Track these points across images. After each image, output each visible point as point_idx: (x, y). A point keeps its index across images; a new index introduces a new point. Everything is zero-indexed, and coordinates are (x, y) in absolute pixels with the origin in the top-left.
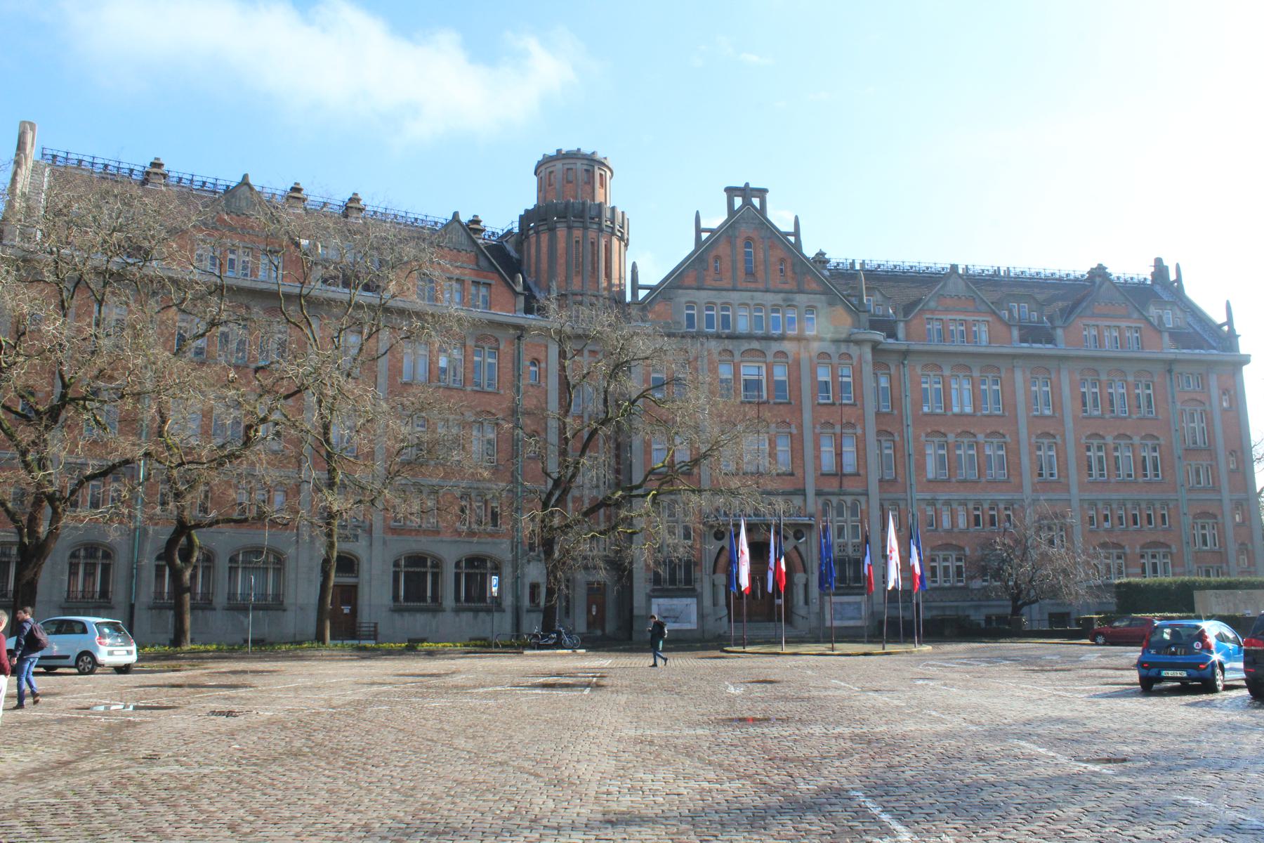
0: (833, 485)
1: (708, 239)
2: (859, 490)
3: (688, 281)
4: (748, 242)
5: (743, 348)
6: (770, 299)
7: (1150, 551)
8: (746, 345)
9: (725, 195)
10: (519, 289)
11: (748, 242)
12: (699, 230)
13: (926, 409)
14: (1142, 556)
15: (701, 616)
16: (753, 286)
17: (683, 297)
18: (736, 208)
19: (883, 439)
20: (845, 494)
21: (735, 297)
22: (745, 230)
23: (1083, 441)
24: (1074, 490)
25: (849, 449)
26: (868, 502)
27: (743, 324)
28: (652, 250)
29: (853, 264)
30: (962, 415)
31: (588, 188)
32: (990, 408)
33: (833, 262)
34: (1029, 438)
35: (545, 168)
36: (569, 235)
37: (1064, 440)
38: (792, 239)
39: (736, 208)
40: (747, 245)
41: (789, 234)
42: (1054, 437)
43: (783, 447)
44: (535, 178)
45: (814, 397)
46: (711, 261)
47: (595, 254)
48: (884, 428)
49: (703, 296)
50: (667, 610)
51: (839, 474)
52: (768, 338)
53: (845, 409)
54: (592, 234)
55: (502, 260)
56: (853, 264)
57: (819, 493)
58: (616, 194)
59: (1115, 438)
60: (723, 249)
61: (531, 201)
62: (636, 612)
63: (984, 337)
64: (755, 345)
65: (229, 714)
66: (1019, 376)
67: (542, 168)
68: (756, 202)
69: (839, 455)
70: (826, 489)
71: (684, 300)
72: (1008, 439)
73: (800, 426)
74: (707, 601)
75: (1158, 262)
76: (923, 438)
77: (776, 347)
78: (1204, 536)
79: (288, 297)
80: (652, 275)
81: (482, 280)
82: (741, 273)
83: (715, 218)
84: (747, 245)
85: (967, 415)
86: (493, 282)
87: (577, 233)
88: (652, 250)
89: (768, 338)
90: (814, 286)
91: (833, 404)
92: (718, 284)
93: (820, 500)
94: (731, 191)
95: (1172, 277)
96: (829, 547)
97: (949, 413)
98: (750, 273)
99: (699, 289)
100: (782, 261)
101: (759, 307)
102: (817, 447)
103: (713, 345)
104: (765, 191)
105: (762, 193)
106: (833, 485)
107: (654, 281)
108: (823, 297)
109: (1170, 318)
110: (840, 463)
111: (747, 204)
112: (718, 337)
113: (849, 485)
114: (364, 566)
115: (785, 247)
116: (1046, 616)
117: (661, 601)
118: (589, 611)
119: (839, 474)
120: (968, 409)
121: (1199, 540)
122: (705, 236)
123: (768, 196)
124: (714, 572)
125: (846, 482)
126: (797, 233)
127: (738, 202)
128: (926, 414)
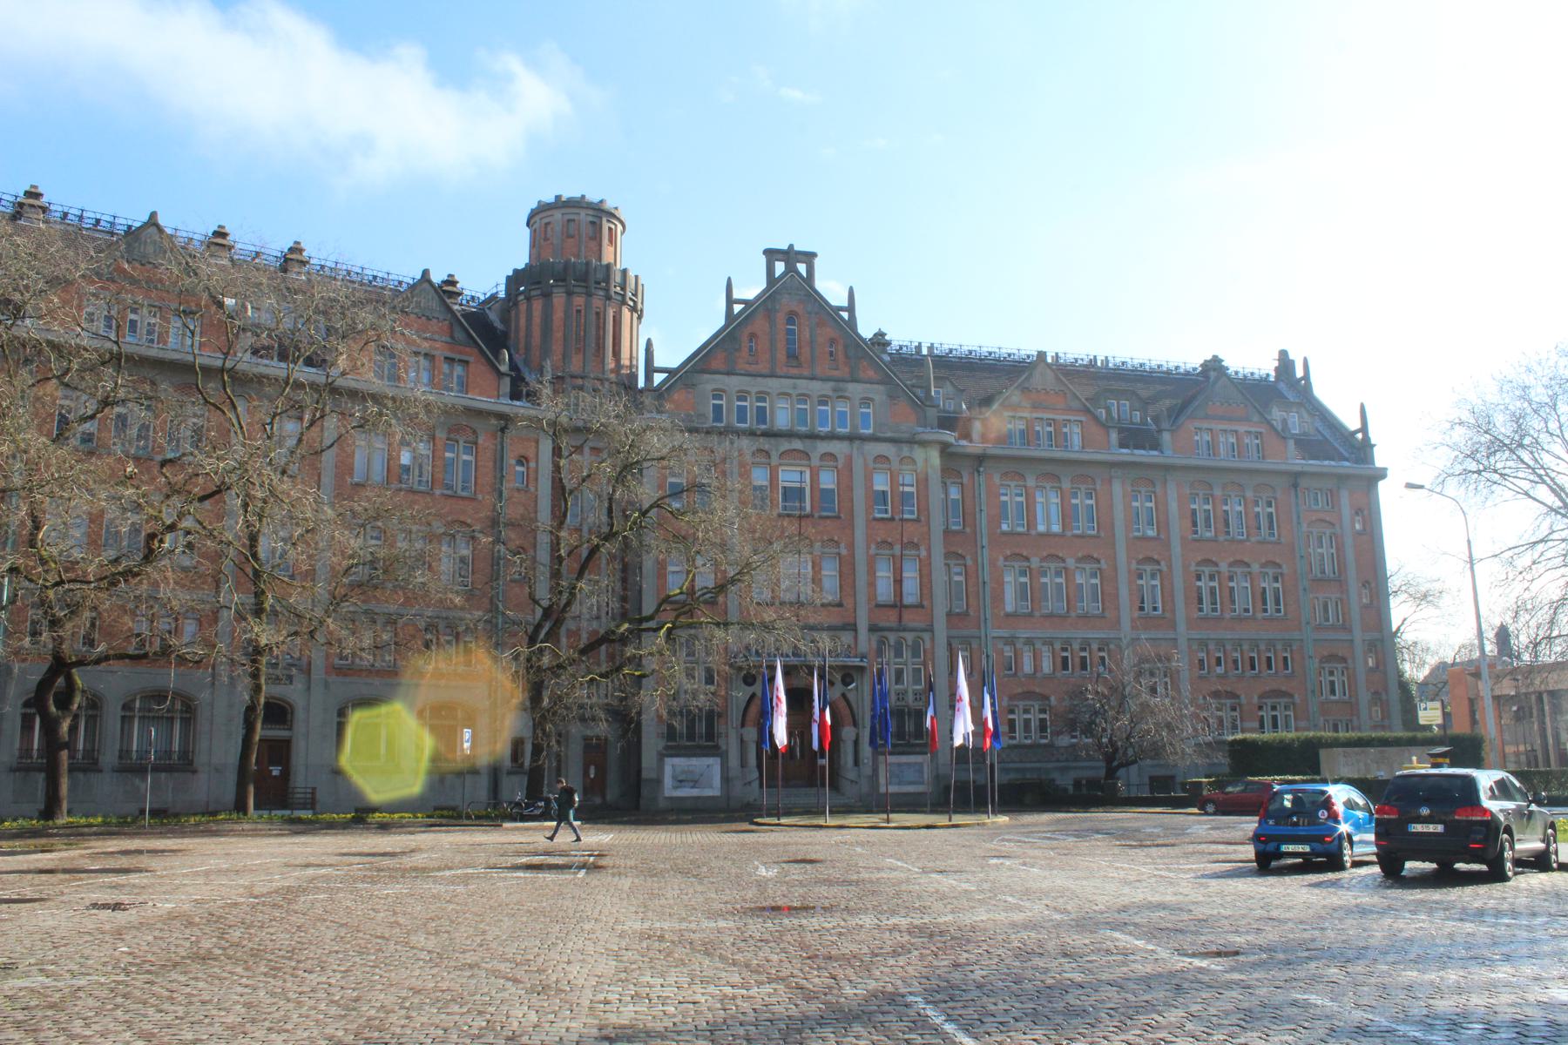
0: (890, 619)
1: (741, 312)
2: (922, 625)
3: (715, 365)
4: (791, 317)
5: (782, 449)
6: (817, 388)
7: (1269, 702)
8: (785, 445)
9: (763, 259)
10: (504, 368)
11: (791, 317)
12: (730, 301)
13: (1005, 527)
14: (1260, 708)
15: (726, 779)
16: (794, 371)
17: (709, 383)
18: (777, 274)
19: (952, 562)
20: (904, 630)
21: (773, 384)
22: (787, 303)
23: (1193, 568)
24: (1182, 627)
25: (911, 575)
26: (932, 639)
27: (782, 418)
28: (672, 324)
29: (919, 347)
30: (1048, 535)
31: (593, 244)
32: (1082, 527)
33: (895, 345)
34: (1129, 563)
35: (540, 218)
36: (569, 304)
37: (1170, 567)
38: (845, 315)
39: (777, 274)
40: (788, 321)
41: (842, 309)
42: (1158, 563)
43: (830, 572)
44: (527, 231)
45: (869, 510)
46: (745, 339)
47: (601, 327)
48: (953, 549)
49: (734, 383)
50: (684, 772)
51: (898, 605)
52: (813, 436)
53: (907, 526)
54: (597, 302)
55: (480, 332)
56: (919, 347)
57: (873, 629)
58: (630, 253)
59: (1231, 565)
60: (760, 325)
61: (521, 259)
62: (645, 775)
63: (1076, 441)
64: (797, 444)
65: (117, 907)
66: (1117, 488)
67: (537, 218)
68: (802, 268)
69: (899, 582)
70: (882, 624)
71: (709, 387)
72: (1103, 565)
73: (851, 546)
74: (734, 761)
75: (1283, 354)
76: (1001, 562)
77: (824, 447)
78: (1332, 683)
79: (207, 370)
80: (671, 355)
81: (457, 357)
82: (781, 355)
83: (751, 287)
84: (788, 321)
85: (1055, 535)
86: (471, 359)
87: (579, 301)
88: (672, 324)
89: (813, 436)
90: (871, 373)
91: (892, 519)
92: (752, 368)
93: (875, 637)
94: (771, 255)
95: (1299, 373)
96: (884, 696)
97: (1069, 534)
98: (792, 356)
99: (728, 374)
100: (832, 341)
101: (803, 398)
102: (872, 572)
103: (745, 443)
104: (814, 255)
105: (809, 257)
106: (890, 619)
107: (674, 362)
108: (881, 388)
109: (1296, 422)
110: (899, 592)
111: (791, 271)
112: (752, 434)
113: (910, 619)
114: (300, 715)
115: (836, 324)
116: (1147, 780)
117: (676, 761)
118: (586, 773)
119: (898, 605)
120: (1056, 528)
121: (1326, 689)
122: (737, 308)
123: (817, 262)
124: (743, 725)
125: (907, 616)
126: (851, 308)
127: (780, 268)
128: (1004, 533)
